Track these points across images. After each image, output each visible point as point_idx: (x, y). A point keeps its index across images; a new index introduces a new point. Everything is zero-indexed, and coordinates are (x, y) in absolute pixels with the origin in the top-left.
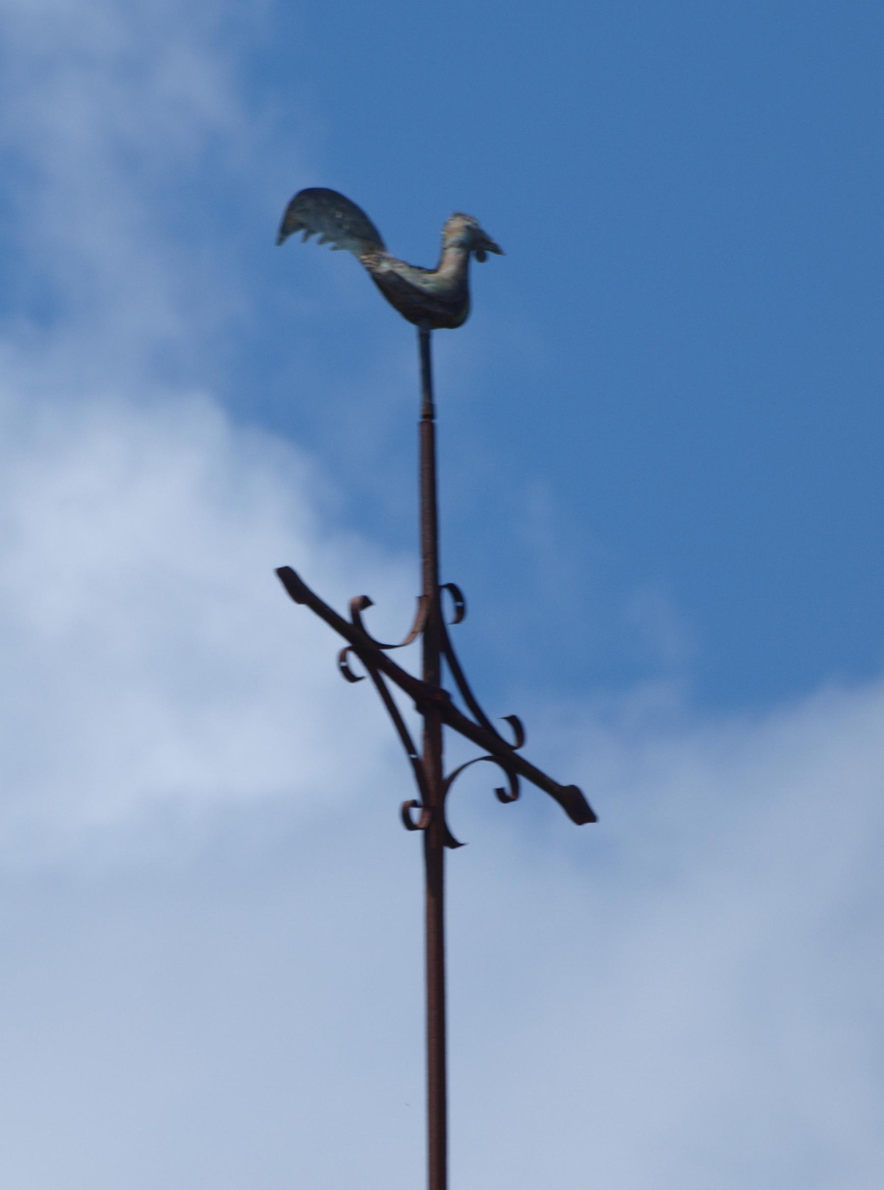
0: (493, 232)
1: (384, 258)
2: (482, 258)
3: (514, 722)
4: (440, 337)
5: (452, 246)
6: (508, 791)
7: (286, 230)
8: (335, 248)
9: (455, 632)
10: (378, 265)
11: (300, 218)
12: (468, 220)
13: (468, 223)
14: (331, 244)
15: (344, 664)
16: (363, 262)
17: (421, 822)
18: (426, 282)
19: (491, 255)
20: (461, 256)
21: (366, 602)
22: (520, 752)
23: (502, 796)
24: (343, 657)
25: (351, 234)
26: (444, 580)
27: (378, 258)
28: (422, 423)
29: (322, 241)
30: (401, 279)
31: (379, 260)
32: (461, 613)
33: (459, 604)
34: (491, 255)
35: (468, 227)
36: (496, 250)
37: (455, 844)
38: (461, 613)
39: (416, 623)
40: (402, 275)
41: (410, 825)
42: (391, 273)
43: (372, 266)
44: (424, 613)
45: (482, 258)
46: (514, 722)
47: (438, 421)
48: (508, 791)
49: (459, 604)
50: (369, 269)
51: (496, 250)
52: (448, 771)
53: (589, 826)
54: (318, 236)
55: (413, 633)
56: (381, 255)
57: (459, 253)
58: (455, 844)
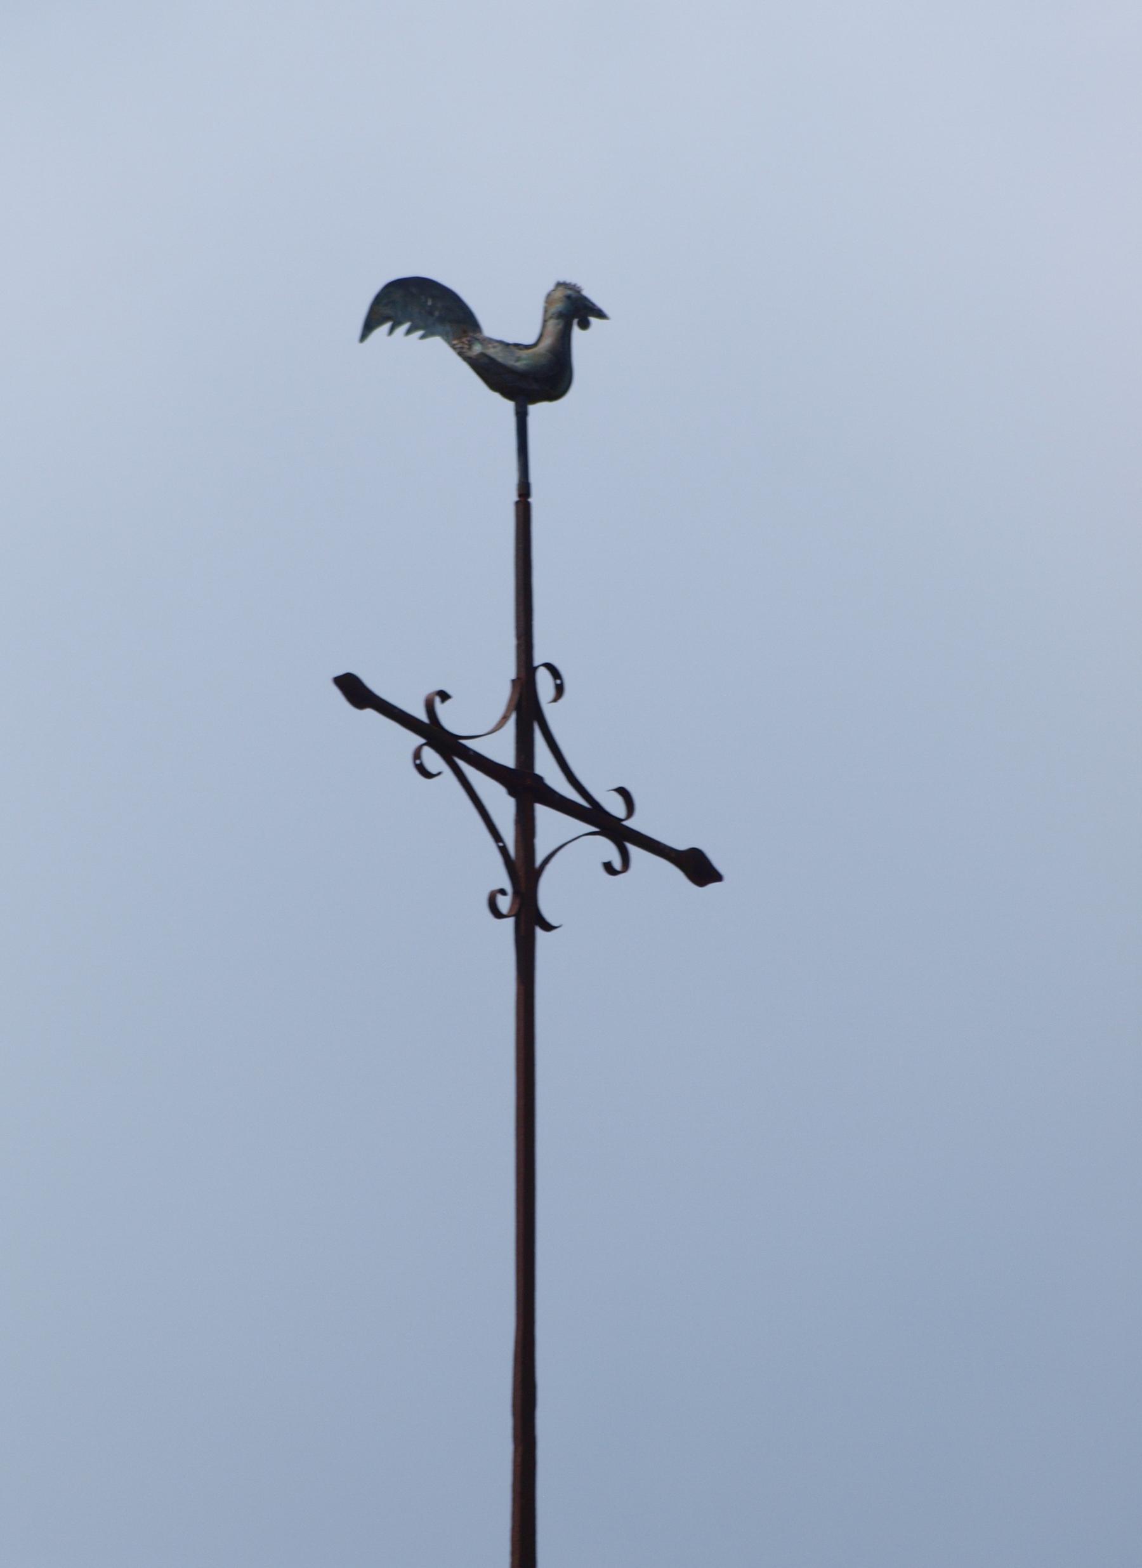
0: (592, 293)
1: (477, 340)
2: (585, 325)
3: (623, 792)
4: (538, 412)
5: (551, 318)
6: (617, 864)
7: (369, 327)
8: (423, 337)
9: (549, 710)
10: (470, 349)
11: (388, 311)
12: (570, 289)
13: (569, 292)
14: (420, 333)
15: (418, 762)
16: (453, 347)
17: (511, 909)
18: (518, 359)
19: (593, 320)
20: (560, 327)
21: (444, 696)
22: (629, 823)
23: (609, 868)
24: (417, 754)
25: (442, 320)
26: (539, 658)
27: (469, 341)
28: (517, 503)
29: (409, 332)
30: (492, 360)
31: (470, 345)
32: (560, 690)
33: (558, 682)
34: (593, 320)
35: (568, 297)
36: (601, 315)
37: (548, 927)
38: (560, 690)
39: (511, 700)
40: (493, 356)
41: (497, 913)
42: (483, 355)
43: (464, 350)
44: (517, 696)
45: (585, 325)
46: (623, 792)
47: (533, 500)
48: (617, 864)
49: (558, 682)
50: (460, 354)
51: (601, 315)
52: (539, 859)
53: (712, 887)
54: (405, 326)
55: (505, 718)
56: (474, 338)
57: (558, 324)
58: (548, 927)
